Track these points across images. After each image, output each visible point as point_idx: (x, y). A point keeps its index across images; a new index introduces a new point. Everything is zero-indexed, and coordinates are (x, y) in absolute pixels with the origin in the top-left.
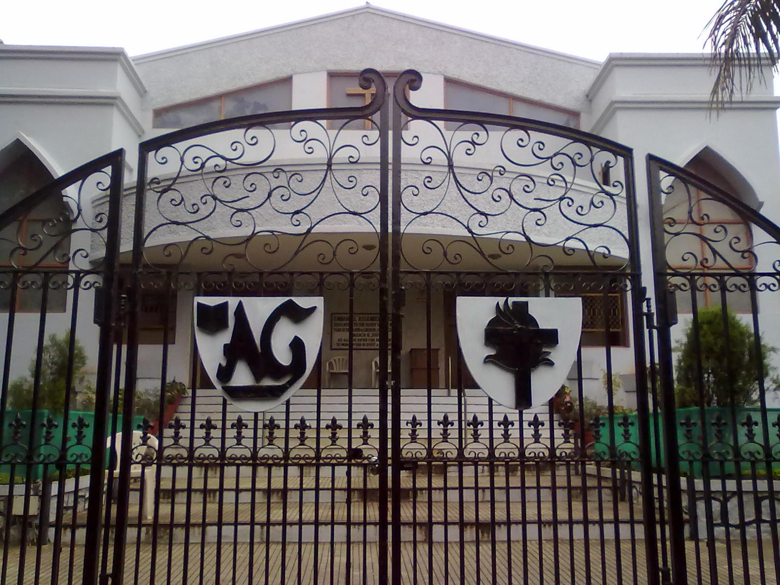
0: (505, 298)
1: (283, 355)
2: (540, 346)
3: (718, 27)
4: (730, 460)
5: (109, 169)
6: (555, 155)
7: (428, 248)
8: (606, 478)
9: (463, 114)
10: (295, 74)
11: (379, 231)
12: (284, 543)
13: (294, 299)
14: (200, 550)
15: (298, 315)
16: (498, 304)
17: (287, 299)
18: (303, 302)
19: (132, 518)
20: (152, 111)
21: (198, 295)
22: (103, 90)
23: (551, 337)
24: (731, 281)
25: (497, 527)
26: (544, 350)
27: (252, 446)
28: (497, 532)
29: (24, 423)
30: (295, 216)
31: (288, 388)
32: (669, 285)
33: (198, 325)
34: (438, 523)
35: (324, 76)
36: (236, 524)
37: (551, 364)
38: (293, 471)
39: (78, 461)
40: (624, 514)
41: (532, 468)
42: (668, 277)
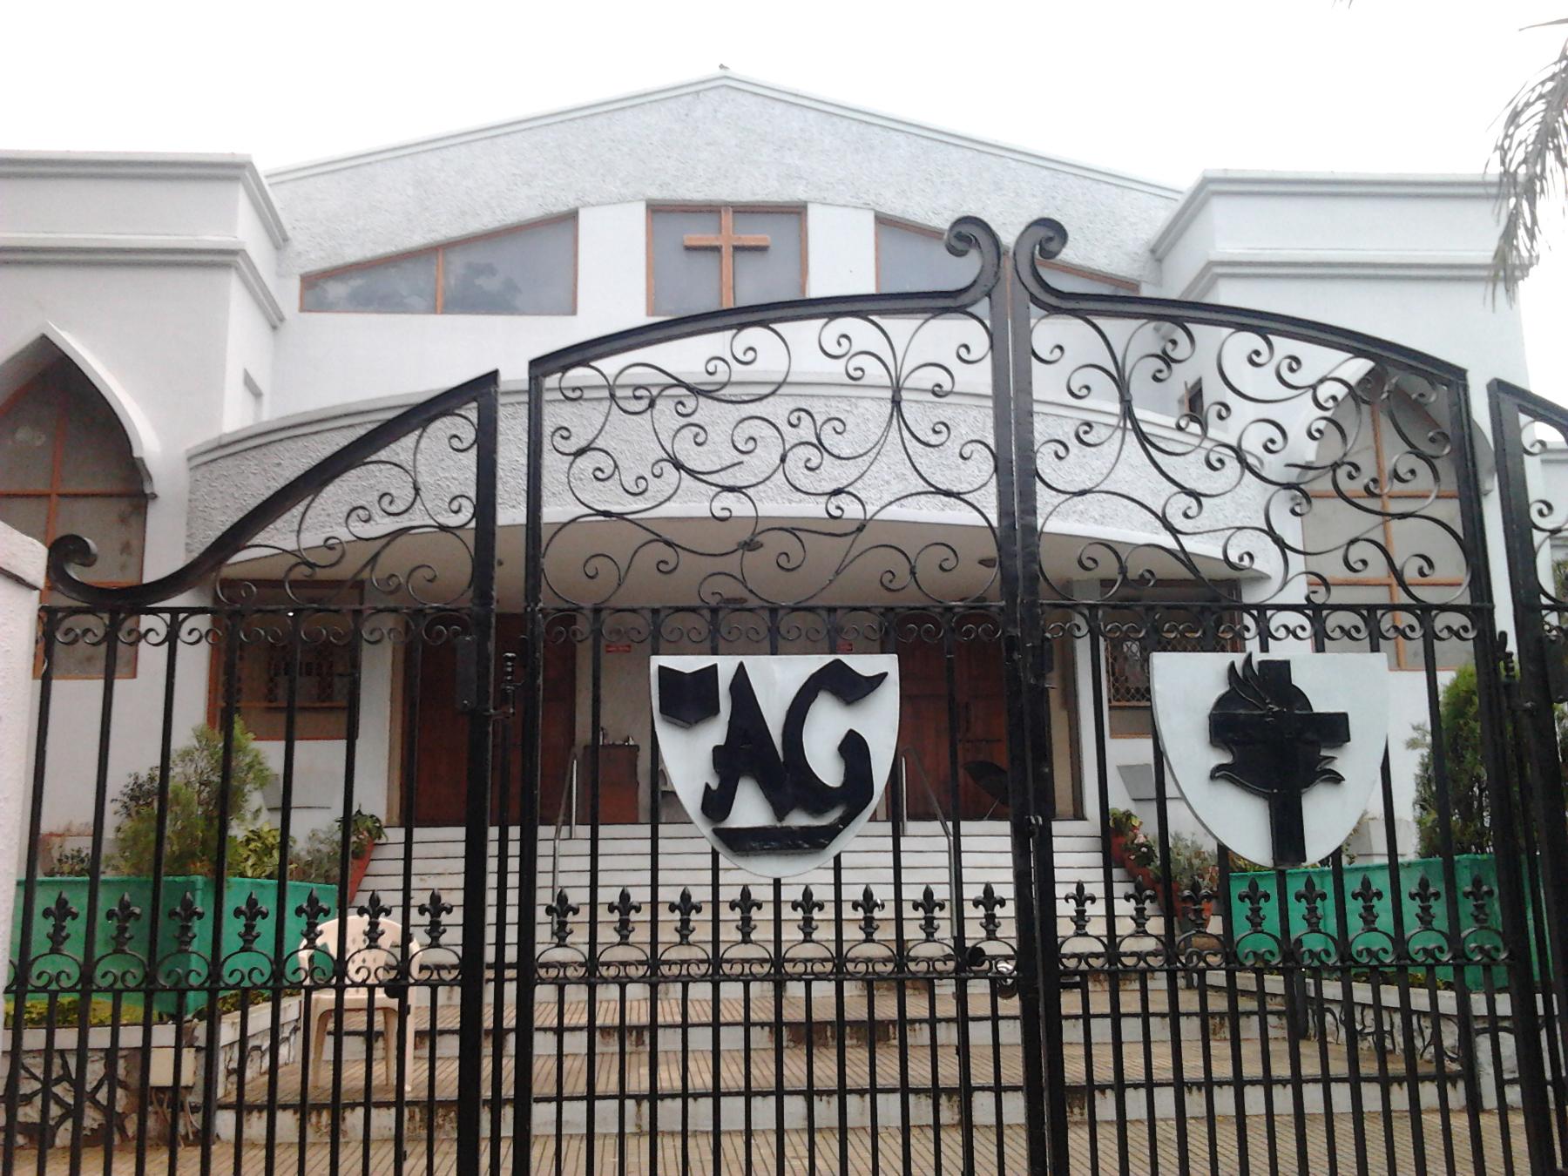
0: (364, 643)
1: (827, 767)
2: (1317, 746)
3: (1510, 132)
4: (1446, 964)
5: (471, 411)
6: (1322, 381)
7: (1089, 558)
8: (1245, 993)
9: (1205, 310)
10: (584, 206)
11: (995, 523)
12: (749, 1133)
13: (845, 659)
14: (296, 1157)
15: (852, 689)
16: (1232, 665)
17: (828, 659)
18: (863, 664)
19: (349, 1091)
20: (298, 278)
21: (657, 653)
22: (211, 237)
23: (1336, 728)
24: (1277, 620)
25: (1097, 1094)
26: (1324, 753)
27: (1105, 933)
28: (1097, 1103)
29: (137, 911)
30: (835, 501)
31: (840, 831)
32: (1547, 627)
33: (662, 710)
34: (982, 1089)
35: (640, 210)
36: (559, 1099)
37: (1337, 779)
38: (851, 989)
39: (54, 987)
40: (1310, 1067)
41: (1102, 977)
42: (1544, 612)
